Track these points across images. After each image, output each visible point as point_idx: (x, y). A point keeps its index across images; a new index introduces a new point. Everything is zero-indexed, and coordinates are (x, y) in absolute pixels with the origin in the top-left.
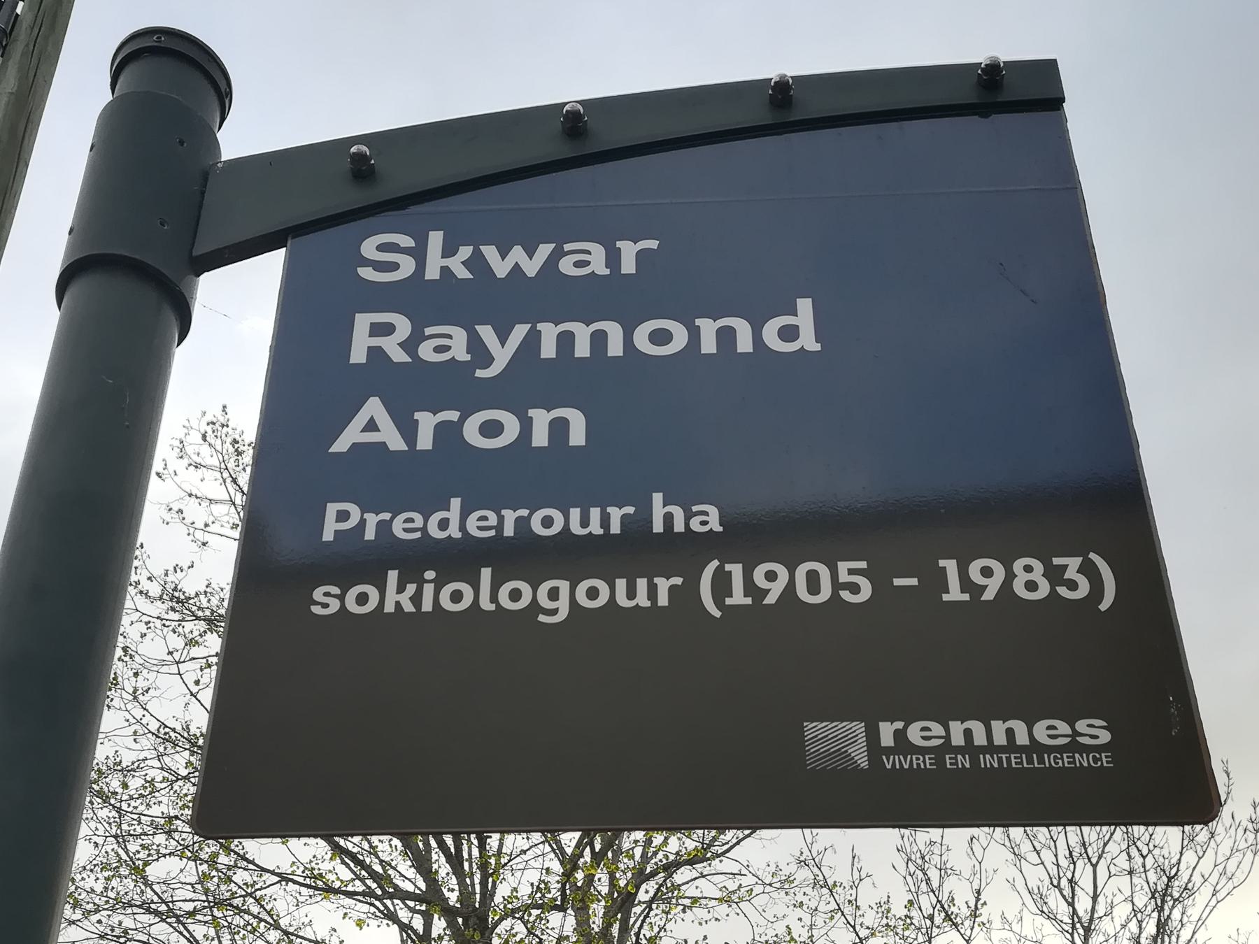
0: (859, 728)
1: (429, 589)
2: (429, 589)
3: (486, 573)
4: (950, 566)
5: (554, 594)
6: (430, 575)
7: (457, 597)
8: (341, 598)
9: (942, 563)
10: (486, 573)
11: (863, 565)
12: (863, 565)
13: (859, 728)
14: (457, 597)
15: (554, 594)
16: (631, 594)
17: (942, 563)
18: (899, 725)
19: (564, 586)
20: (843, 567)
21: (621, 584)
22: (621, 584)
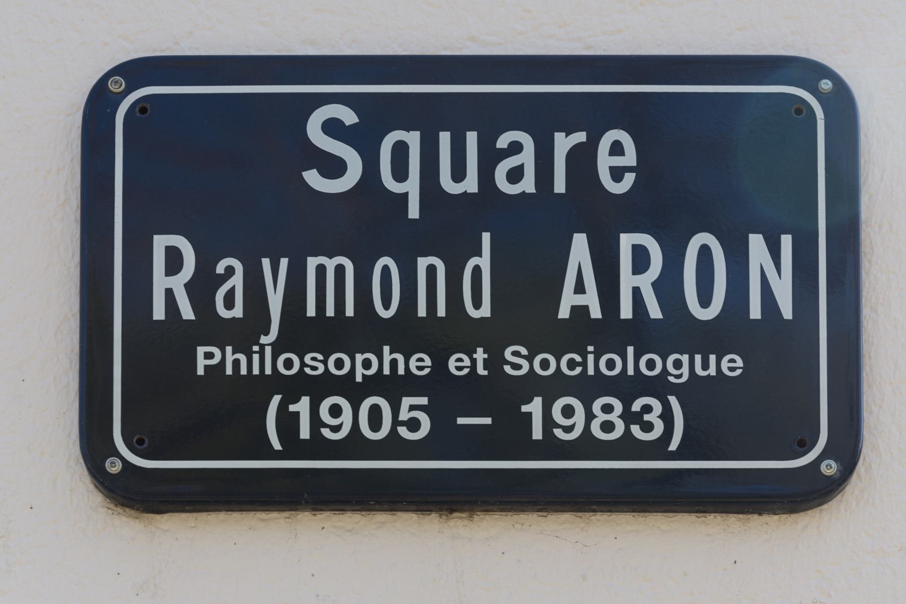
0: (633, 163)
1: (591, 358)
2: (591, 358)
3: (630, 350)
4: (481, 371)
5: (678, 364)
6: (591, 348)
7: (611, 365)
8: (325, 362)
9: (486, 373)
10: (630, 350)
11: (424, 401)
12: (424, 401)
13: (633, 163)
14: (611, 365)
15: (678, 364)
16: (705, 366)
17: (486, 373)
18: (580, 137)
19: (685, 358)
20: (407, 402)
21: (401, 371)
22: (401, 371)
